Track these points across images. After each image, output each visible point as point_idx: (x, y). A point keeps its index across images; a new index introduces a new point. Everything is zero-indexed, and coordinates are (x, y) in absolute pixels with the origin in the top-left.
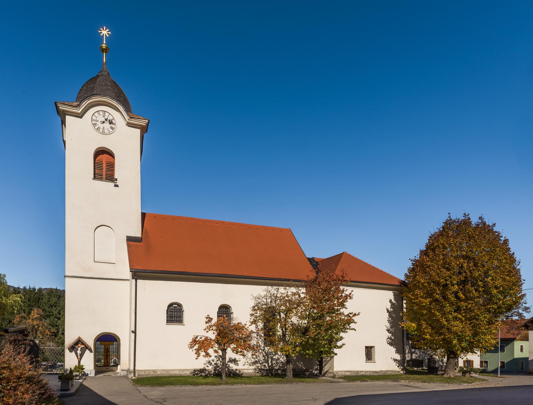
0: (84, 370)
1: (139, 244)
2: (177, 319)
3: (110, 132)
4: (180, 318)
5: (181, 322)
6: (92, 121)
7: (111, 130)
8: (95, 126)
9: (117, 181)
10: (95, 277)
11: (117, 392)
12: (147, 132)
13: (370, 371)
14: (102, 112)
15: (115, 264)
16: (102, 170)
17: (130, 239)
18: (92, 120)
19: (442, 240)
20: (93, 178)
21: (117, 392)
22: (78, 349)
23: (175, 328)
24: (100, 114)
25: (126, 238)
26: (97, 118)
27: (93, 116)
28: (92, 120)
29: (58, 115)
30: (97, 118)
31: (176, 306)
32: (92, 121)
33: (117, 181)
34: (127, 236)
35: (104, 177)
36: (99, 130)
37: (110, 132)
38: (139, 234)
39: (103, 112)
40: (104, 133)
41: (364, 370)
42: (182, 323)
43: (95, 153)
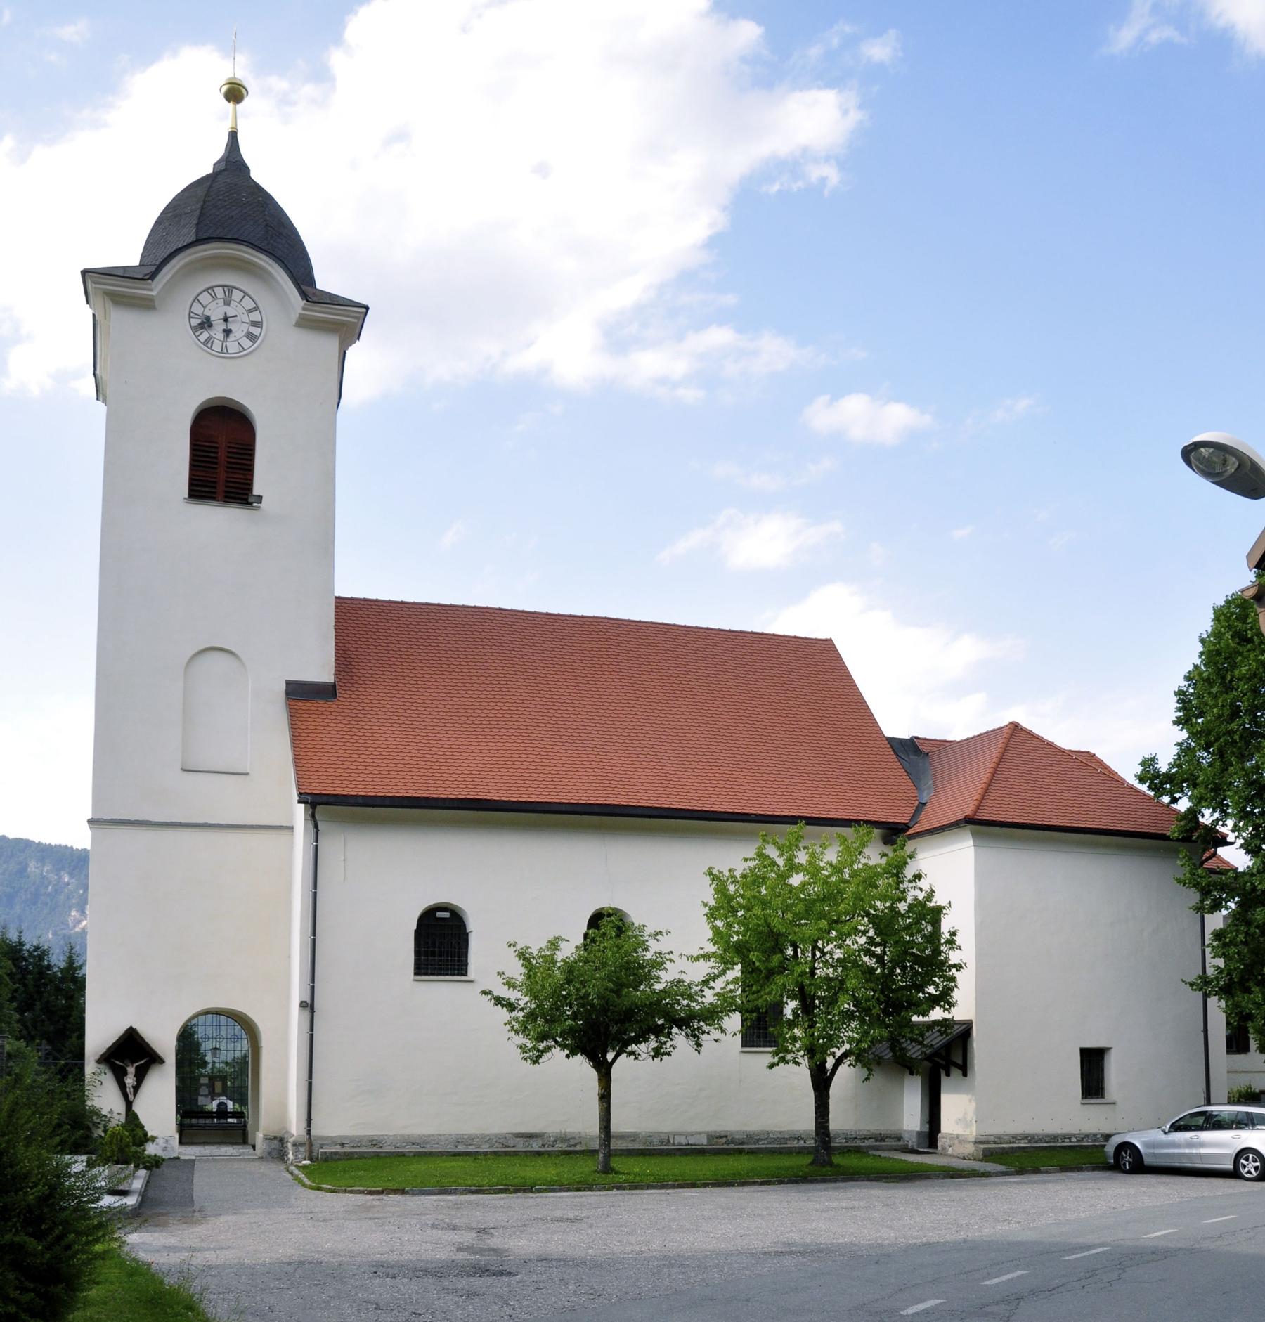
0: (1191, 670)
1: (325, 705)
2: (448, 960)
3: (244, 350)
4: (459, 957)
5: (464, 972)
6: (191, 320)
7: (246, 343)
8: (197, 334)
9: (261, 503)
10: (183, 821)
11: (721, 1137)
12: (358, 339)
13: (1095, 1135)
14: (221, 288)
15: (247, 774)
16: (216, 468)
17: (298, 692)
18: (192, 315)
19: (84, 1192)
20: (187, 496)
21: (721, 1137)
22: (126, 1070)
23: (441, 990)
24: (215, 298)
25: (284, 687)
26: (204, 307)
27: (194, 304)
28: (192, 315)
29: (88, 303)
30: (204, 307)
31: (447, 915)
32: (190, 317)
33: (261, 503)
34: (288, 683)
35: (221, 488)
36: (209, 346)
37: (244, 350)
38: (325, 674)
39: (226, 289)
40: (227, 353)
41: (1078, 1132)
42: (466, 974)
43: (199, 410)
